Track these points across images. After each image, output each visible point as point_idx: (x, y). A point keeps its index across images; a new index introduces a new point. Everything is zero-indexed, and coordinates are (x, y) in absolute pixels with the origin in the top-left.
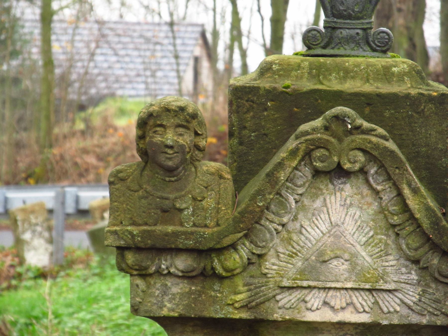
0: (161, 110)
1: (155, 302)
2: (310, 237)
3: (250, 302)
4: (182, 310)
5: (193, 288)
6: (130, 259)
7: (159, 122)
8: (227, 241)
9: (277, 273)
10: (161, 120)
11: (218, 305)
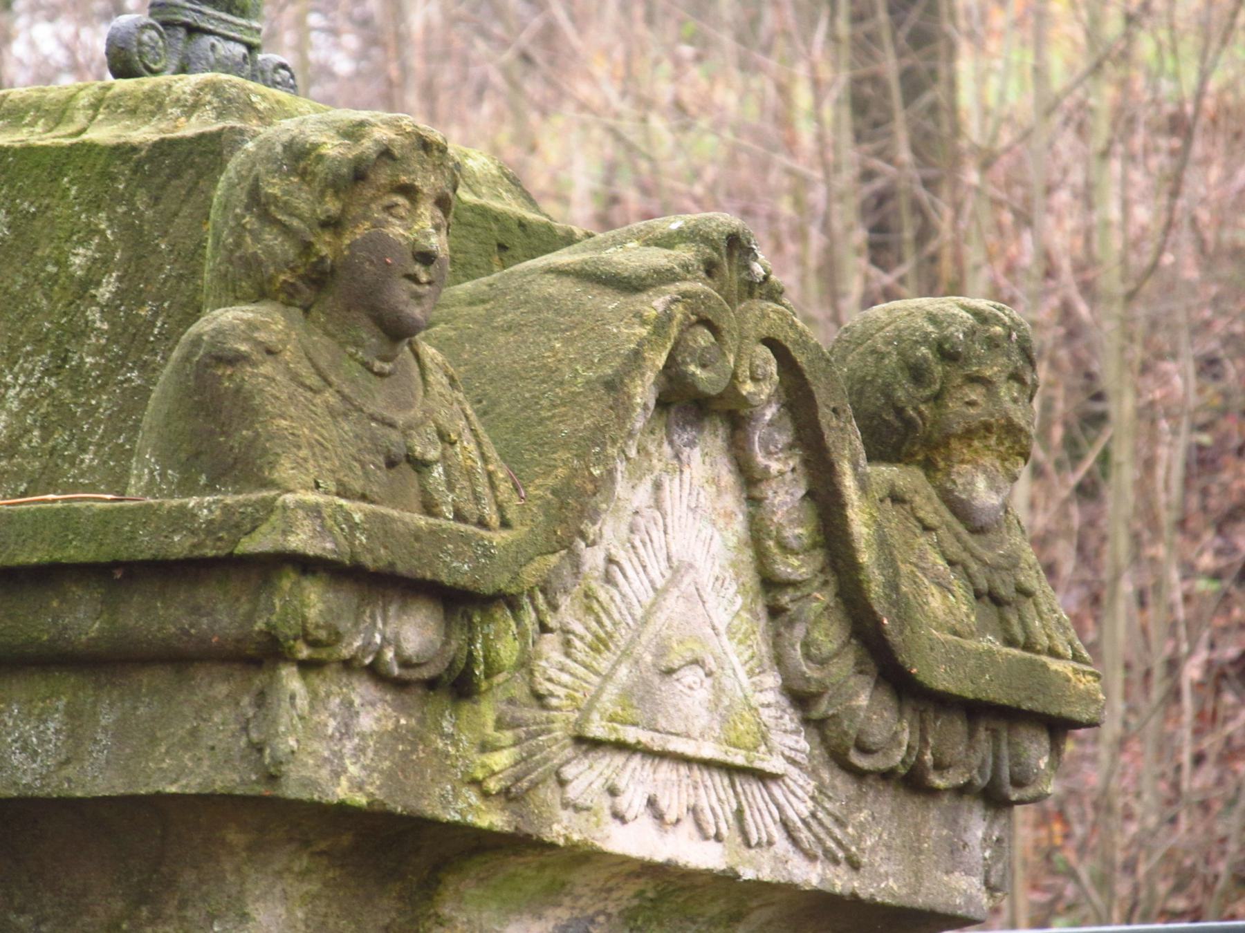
0: (407, 142)
1: (326, 754)
2: (630, 594)
3: (518, 779)
4: (379, 788)
5: (403, 721)
6: (314, 606)
7: (404, 179)
8: (531, 574)
9: (568, 697)
10: (410, 173)
11: (450, 780)
